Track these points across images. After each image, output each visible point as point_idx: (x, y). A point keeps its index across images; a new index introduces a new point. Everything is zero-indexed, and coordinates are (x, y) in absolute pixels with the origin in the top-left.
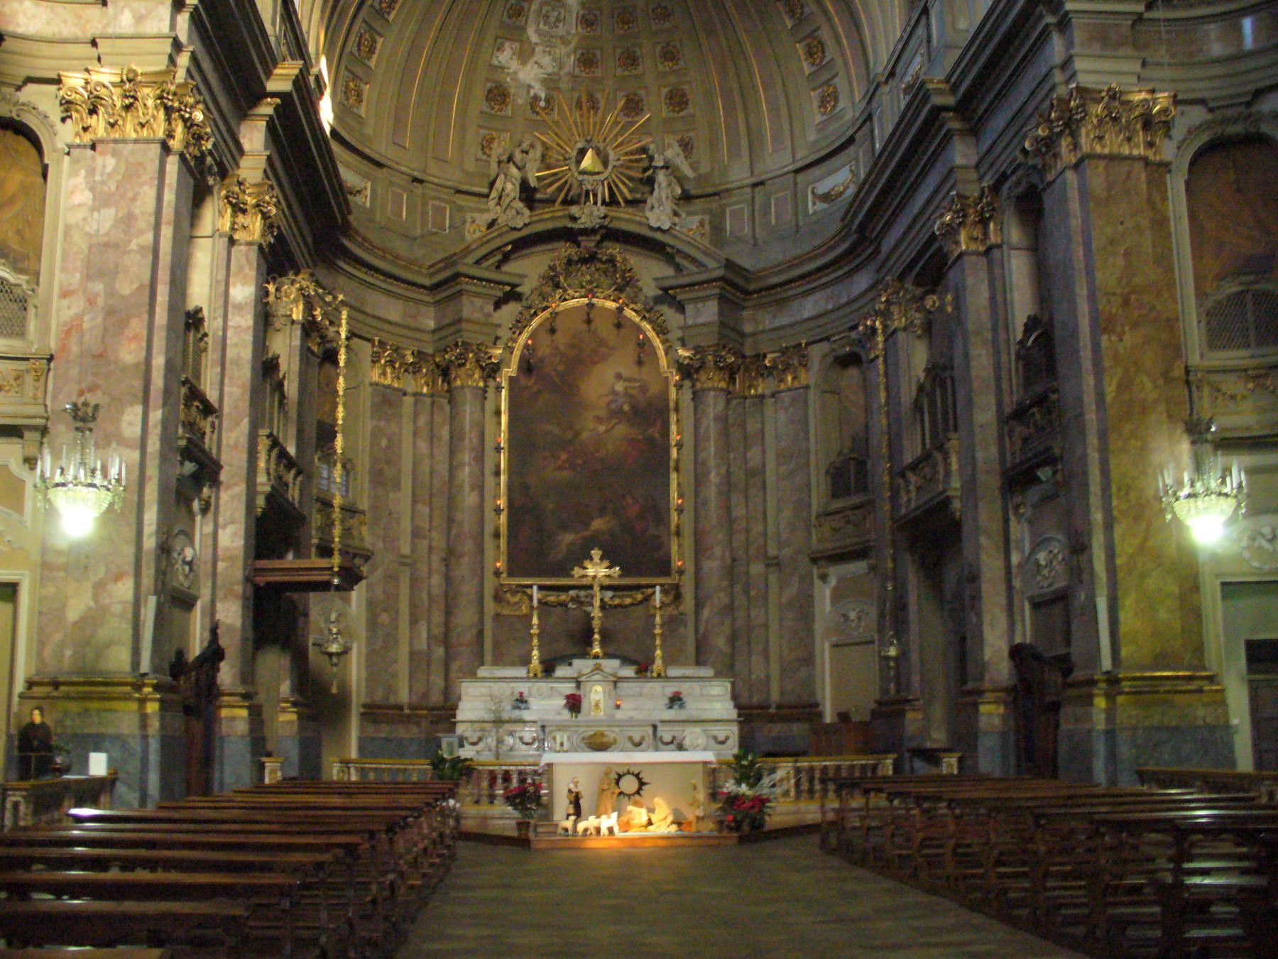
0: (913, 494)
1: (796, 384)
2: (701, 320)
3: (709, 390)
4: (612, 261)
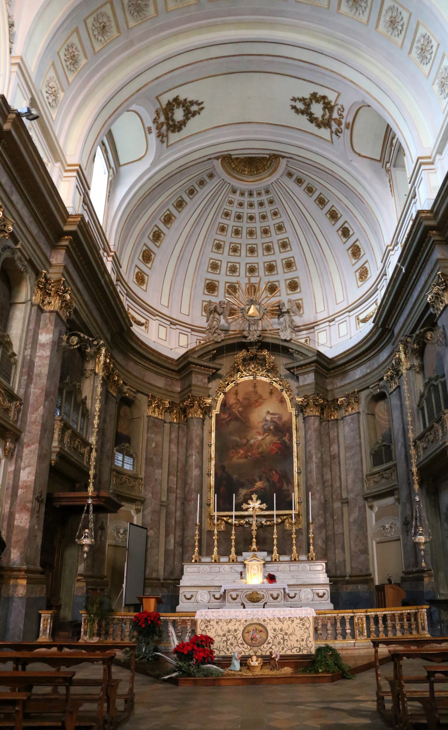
0: (422, 452)
1: (354, 412)
2: (306, 383)
3: (311, 416)
4: (264, 359)
